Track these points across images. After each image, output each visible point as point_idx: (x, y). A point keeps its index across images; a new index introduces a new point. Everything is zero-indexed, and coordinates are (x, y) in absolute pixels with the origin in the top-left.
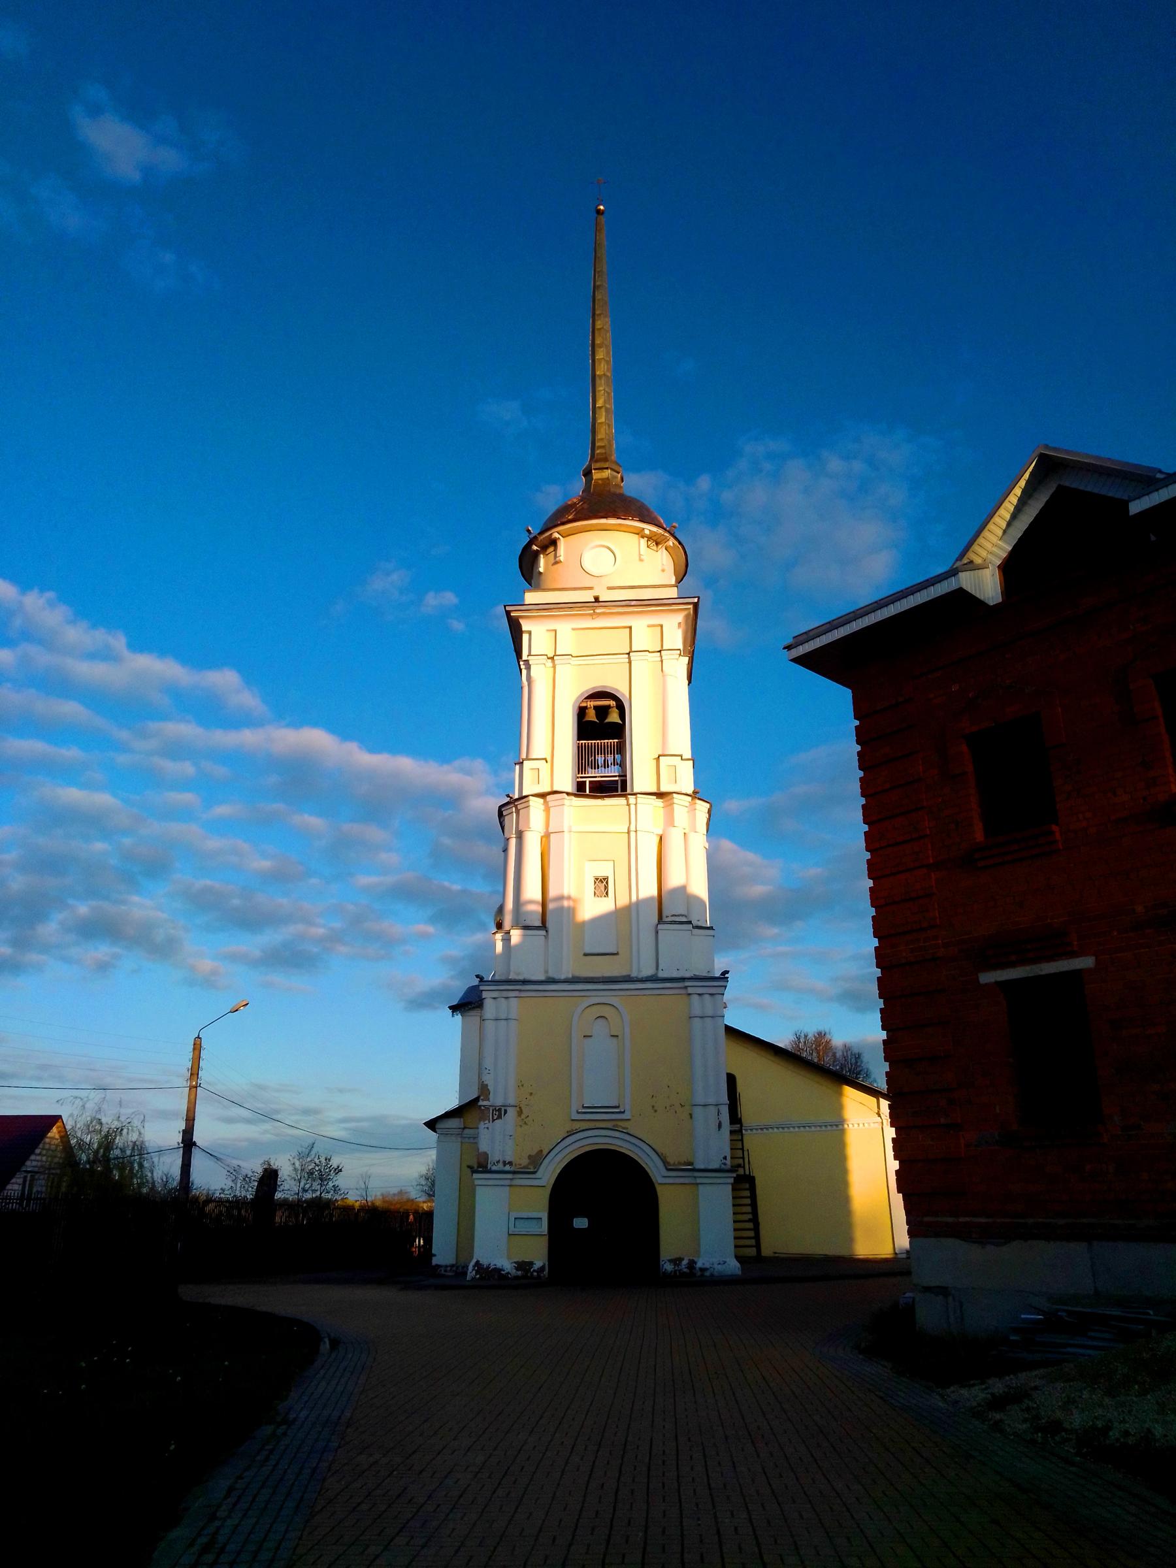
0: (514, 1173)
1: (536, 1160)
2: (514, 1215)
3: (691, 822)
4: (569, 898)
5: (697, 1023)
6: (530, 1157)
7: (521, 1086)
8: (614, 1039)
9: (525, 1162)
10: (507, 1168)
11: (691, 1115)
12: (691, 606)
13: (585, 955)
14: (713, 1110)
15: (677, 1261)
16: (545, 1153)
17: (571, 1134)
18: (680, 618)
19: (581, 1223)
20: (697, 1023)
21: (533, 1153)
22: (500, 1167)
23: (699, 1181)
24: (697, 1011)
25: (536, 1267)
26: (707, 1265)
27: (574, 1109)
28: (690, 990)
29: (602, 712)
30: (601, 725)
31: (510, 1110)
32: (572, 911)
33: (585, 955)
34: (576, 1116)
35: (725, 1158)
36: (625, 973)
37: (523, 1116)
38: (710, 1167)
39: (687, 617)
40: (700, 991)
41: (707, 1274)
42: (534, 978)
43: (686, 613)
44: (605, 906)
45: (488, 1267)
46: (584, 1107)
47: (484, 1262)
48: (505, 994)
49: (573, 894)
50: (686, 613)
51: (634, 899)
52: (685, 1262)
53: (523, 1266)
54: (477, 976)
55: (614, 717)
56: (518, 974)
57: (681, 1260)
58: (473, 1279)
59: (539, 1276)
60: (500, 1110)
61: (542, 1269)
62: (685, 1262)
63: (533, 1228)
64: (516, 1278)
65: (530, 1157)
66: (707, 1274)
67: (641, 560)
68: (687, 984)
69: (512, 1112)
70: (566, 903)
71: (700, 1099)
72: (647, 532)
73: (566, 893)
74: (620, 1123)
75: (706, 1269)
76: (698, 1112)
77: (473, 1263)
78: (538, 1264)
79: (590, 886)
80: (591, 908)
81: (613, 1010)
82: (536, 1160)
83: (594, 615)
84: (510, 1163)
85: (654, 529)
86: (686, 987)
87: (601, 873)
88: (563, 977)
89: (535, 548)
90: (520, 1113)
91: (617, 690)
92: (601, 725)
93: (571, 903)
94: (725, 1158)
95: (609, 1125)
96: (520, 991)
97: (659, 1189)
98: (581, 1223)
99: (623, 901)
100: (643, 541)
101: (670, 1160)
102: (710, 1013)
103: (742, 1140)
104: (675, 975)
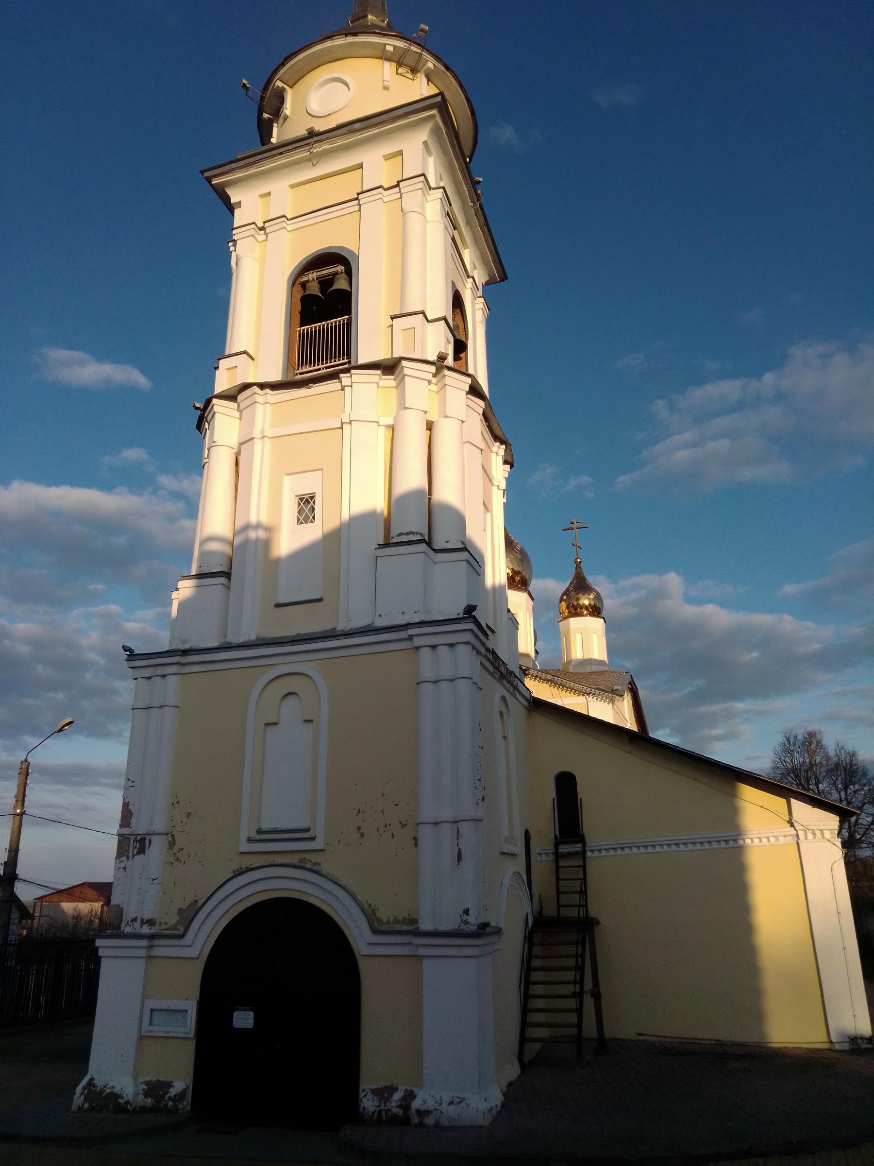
0: (152, 937)
1: (189, 914)
2: (151, 1004)
3: (459, 415)
4: (258, 526)
5: (427, 688)
6: (180, 911)
7: (176, 804)
8: (308, 725)
9: (173, 919)
10: (146, 930)
11: (415, 839)
12: (434, 112)
13: (278, 606)
14: (447, 830)
15: (384, 1093)
16: (200, 903)
17: (239, 873)
18: (423, 134)
19: (244, 1019)
20: (427, 688)
21: (185, 906)
22: (136, 928)
23: (422, 952)
24: (427, 673)
25: (173, 1092)
26: (430, 1105)
27: (244, 836)
28: (417, 642)
29: (326, 283)
30: (324, 299)
31: (156, 840)
32: (267, 544)
33: (278, 606)
34: (245, 847)
35: (466, 912)
36: (329, 627)
37: (176, 849)
38: (442, 928)
39: (435, 132)
40: (451, 639)
41: (430, 1121)
42: (203, 645)
43: (429, 126)
44: (313, 533)
45: (102, 1091)
46: (259, 832)
47: (99, 1082)
48: (160, 671)
49: (264, 519)
50: (429, 126)
51: (345, 516)
52: (397, 1096)
53: (157, 1089)
54: (125, 649)
55: (341, 284)
56: (184, 641)
57: (392, 1090)
58: (80, 1109)
59: (176, 1107)
60: (143, 840)
61: (182, 1095)
62: (397, 1096)
63: (176, 1030)
64: (144, 1109)
65: (180, 911)
66: (430, 1121)
67: (386, 88)
68: (411, 632)
69: (157, 847)
70: (252, 535)
71: (428, 813)
72: (390, 48)
73: (253, 519)
74: (307, 856)
75: (427, 1113)
76: (426, 834)
77: (84, 1082)
78: (178, 1087)
79: (289, 509)
80: (290, 538)
81: (302, 678)
82: (189, 914)
83: (313, 160)
84: (151, 922)
85: (401, 44)
86: (411, 637)
87: (305, 491)
88: (241, 640)
89: (266, 116)
90: (172, 843)
91: (343, 248)
92: (324, 299)
93: (261, 534)
94: (466, 912)
95: (294, 859)
96: (183, 665)
97: (366, 969)
98: (244, 1019)
99: (332, 524)
100: (389, 68)
101: (383, 914)
102: (446, 674)
103: (584, 867)
104: (400, 620)
